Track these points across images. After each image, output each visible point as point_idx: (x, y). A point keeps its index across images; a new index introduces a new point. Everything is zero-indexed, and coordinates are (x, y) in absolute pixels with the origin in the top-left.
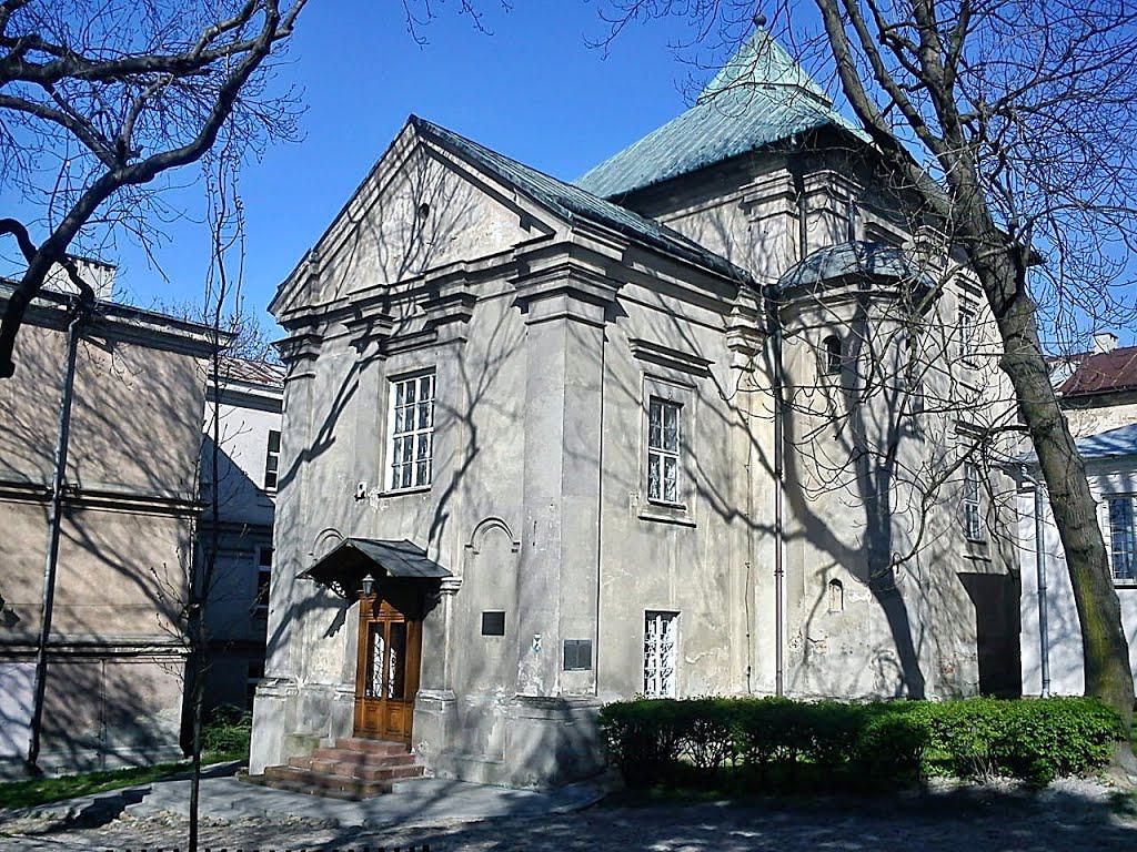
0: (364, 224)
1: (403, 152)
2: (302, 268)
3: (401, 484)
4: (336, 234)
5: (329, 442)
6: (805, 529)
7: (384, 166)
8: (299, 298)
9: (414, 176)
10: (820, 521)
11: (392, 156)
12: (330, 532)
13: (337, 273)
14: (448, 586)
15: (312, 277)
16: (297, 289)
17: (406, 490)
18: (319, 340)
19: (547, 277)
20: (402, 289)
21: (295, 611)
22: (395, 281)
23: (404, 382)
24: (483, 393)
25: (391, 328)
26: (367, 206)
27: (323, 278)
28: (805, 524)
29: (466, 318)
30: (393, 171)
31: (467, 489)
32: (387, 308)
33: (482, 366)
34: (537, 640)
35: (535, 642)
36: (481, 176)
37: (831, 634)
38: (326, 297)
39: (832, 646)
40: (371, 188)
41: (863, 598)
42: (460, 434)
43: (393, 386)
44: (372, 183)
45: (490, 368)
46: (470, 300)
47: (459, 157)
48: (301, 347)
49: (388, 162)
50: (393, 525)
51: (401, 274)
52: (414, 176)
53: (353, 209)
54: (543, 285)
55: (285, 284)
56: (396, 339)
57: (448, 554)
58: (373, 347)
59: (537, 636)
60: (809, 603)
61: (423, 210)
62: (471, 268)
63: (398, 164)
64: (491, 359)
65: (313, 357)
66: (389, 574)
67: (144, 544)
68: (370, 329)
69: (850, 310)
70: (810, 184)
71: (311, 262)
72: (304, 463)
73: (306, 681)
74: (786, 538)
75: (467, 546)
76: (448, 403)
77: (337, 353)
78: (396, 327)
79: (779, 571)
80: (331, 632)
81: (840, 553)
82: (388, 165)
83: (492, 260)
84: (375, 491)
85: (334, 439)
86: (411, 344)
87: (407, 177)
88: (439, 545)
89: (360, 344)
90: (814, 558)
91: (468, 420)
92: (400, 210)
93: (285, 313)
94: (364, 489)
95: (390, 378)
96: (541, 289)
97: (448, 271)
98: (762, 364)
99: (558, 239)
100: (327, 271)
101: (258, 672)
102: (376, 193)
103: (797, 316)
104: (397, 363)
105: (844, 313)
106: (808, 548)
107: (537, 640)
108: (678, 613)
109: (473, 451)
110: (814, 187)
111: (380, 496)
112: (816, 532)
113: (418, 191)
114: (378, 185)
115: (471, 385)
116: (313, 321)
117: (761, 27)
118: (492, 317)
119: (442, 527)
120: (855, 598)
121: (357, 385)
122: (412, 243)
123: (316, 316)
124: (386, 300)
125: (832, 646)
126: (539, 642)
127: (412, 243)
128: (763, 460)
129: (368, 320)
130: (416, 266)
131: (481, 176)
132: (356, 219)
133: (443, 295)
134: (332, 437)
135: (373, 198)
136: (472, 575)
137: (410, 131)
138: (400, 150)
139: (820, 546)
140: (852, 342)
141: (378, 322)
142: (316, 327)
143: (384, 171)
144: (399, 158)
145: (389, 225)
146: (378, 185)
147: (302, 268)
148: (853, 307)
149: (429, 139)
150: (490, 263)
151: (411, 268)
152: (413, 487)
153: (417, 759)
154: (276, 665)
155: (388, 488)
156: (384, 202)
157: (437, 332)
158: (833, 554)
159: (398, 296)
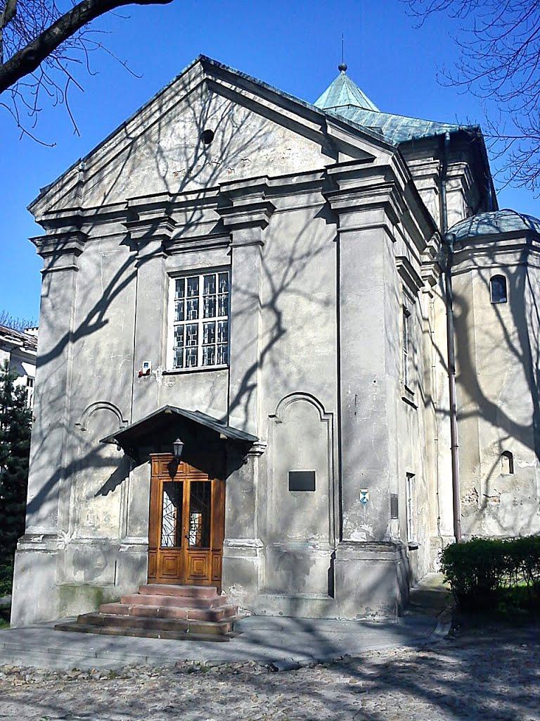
0: (139, 141)
1: (190, 83)
2: (70, 175)
3: (216, 363)
4: (108, 149)
5: (100, 324)
6: (481, 412)
7: (168, 94)
8: (63, 200)
9: (197, 105)
10: (495, 406)
11: (178, 86)
12: (95, 407)
13: (106, 181)
14: (258, 449)
15: (80, 184)
16: (68, 188)
17: (195, 369)
18: (85, 238)
19: (367, 193)
20: (182, 199)
21: (62, 473)
22: (176, 192)
23: (217, 274)
24: (288, 284)
25: (172, 231)
26: (147, 125)
27: (91, 183)
28: (230, 440)
29: (263, 224)
30: (177, 99)
31: (274, 364)
32: (169, 212)
33: (286, 261)
34: (365, 494)
35: (362, 496)
36: (285, 113)
37: (504, 492)
38: (91, 201)
39: (506, 498)
40: (153, 110)
41: (531, 465)
42: (262, 323)
43: (173, 282)
44: (155, 107)
45: (296, 263)
46: (271, 210)
47: (253, 93)
48: (65, 243)
49: (173, 90)
50: (199, 398)
51: (183, 184)
52: (197, 105)
53: (130, 128)
54: (360, 200)
55: (51, 187)
56: (176, 240)
57: (254, 419)
58: (154, 246)
59: (363, 491)
60: (485, 470)
61: (207, 137)
62: (275, 183)
63: (183, 93)
64: (296, 255)
65: (77, 252)
66: (222, 436)
67: (42, 387)
68: (153, 230)
69: (515, 256)
70: (451, 171)
71: (80, 171)
72: (70, 344)
73: (74, 537)
74: (461, 417)
75: (270, 416)
76: (253, 290)
77: (101, 256)
78: (177, 231)
79: (454, 447)
80: (104, 491)
81: (514, 430)
82: (173, 93)
83: (296, 178)
84: (161, 370)
85: (106, 322)
86: (200, 245)
87: (189, 105)
88: (246, 410)
89: (136, 245)
90: (489, 433)
91: (271, 305)
92: (182, 131)
93: (46, 213)
94: (150, 367)
95: (169, 274)
96: (355, 203)
97: (252, 184)
98: (439, 291)
99: (377, 163)
100: (96, 178)
101: (20, 530)
102: (158, 115)
103: (471, 258)
104: (173, 263)
105: (511, 259)
106: (484, 426)
107: (365, 494)
108: (414, 475)
109: (279, 332)
110: (454, 173)
111: (165, 373)
112: (491, 413)
113: (201, 117)
114: (160, 109)
115: (274, 277)
116: (78, 221)
117: (343, 72)
118: (294, 224)
119: (249, 396)
120: (524, 464)
121: (135, 274)
122: (197, 159)
123: (83, 217)
124: (169, 207)
125: (506, 498)
126: (367, 496)
127: (197, 159)
128: (442, 361)
129: (145, 225)
130: (204, 177)
131: (285, 113)
132: (132, 136)
133: (241, 207)
134: (103, 319)
135: (152, 120)
136: (282, 438)
137: (198, 68)
138: (187, 82)
139: (495, 424)
140: (518, 278)
141: (163, 224)
142: (79, 227)
143: (167, 98)
144: (184, 88)
145: (168, 141)
146: (160, 109)
147: (70, 175)
148: (518, 256)
149: (216, 75)
150: (294, 181)
151: (196, 179)
152: (200, 367)
153: (229, 600)
154: (35, 527)
155: (170, 368)
156: (163, 123)
157: (231, 236)
158: (506, 429)
159: (180, 204)
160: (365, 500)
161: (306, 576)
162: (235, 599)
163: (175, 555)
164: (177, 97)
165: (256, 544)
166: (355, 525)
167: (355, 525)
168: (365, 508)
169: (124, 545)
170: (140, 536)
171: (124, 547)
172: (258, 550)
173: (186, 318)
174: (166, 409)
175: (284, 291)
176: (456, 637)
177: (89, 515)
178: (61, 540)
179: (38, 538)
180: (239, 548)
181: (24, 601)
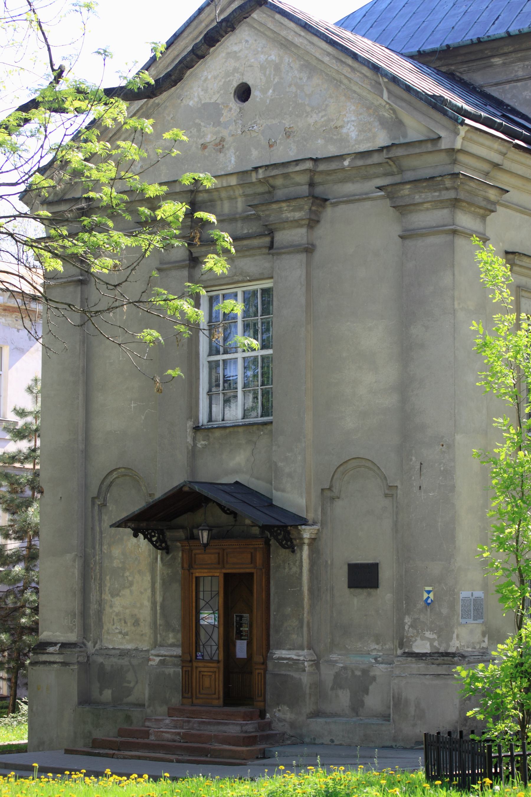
35: (426, 595)
126: (431, 595)
160: (429, 601)
161: (365, 696)
162: (280, 724)
163: (212, 670)
164: (270, 182)
165: (305, 657)
166: (418, 632)
167: (418, 632)
168: (429, 610)
169: (154, 658)
170: (172, 645)
171: (154, 660)
172: (306, 664)
173: (270, 383)
174: (184, 485)
175: (269, 245)
176: (325, 110)
177: (115, 618)
178: (82, 649)
179: (55, 648)
180: (285, 662)
181: (293, 551)
